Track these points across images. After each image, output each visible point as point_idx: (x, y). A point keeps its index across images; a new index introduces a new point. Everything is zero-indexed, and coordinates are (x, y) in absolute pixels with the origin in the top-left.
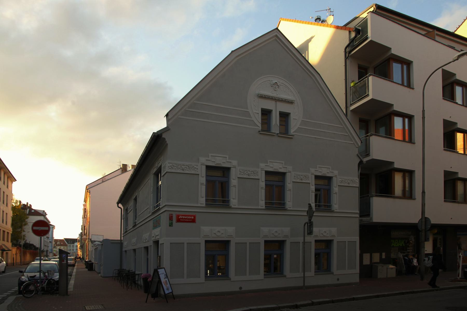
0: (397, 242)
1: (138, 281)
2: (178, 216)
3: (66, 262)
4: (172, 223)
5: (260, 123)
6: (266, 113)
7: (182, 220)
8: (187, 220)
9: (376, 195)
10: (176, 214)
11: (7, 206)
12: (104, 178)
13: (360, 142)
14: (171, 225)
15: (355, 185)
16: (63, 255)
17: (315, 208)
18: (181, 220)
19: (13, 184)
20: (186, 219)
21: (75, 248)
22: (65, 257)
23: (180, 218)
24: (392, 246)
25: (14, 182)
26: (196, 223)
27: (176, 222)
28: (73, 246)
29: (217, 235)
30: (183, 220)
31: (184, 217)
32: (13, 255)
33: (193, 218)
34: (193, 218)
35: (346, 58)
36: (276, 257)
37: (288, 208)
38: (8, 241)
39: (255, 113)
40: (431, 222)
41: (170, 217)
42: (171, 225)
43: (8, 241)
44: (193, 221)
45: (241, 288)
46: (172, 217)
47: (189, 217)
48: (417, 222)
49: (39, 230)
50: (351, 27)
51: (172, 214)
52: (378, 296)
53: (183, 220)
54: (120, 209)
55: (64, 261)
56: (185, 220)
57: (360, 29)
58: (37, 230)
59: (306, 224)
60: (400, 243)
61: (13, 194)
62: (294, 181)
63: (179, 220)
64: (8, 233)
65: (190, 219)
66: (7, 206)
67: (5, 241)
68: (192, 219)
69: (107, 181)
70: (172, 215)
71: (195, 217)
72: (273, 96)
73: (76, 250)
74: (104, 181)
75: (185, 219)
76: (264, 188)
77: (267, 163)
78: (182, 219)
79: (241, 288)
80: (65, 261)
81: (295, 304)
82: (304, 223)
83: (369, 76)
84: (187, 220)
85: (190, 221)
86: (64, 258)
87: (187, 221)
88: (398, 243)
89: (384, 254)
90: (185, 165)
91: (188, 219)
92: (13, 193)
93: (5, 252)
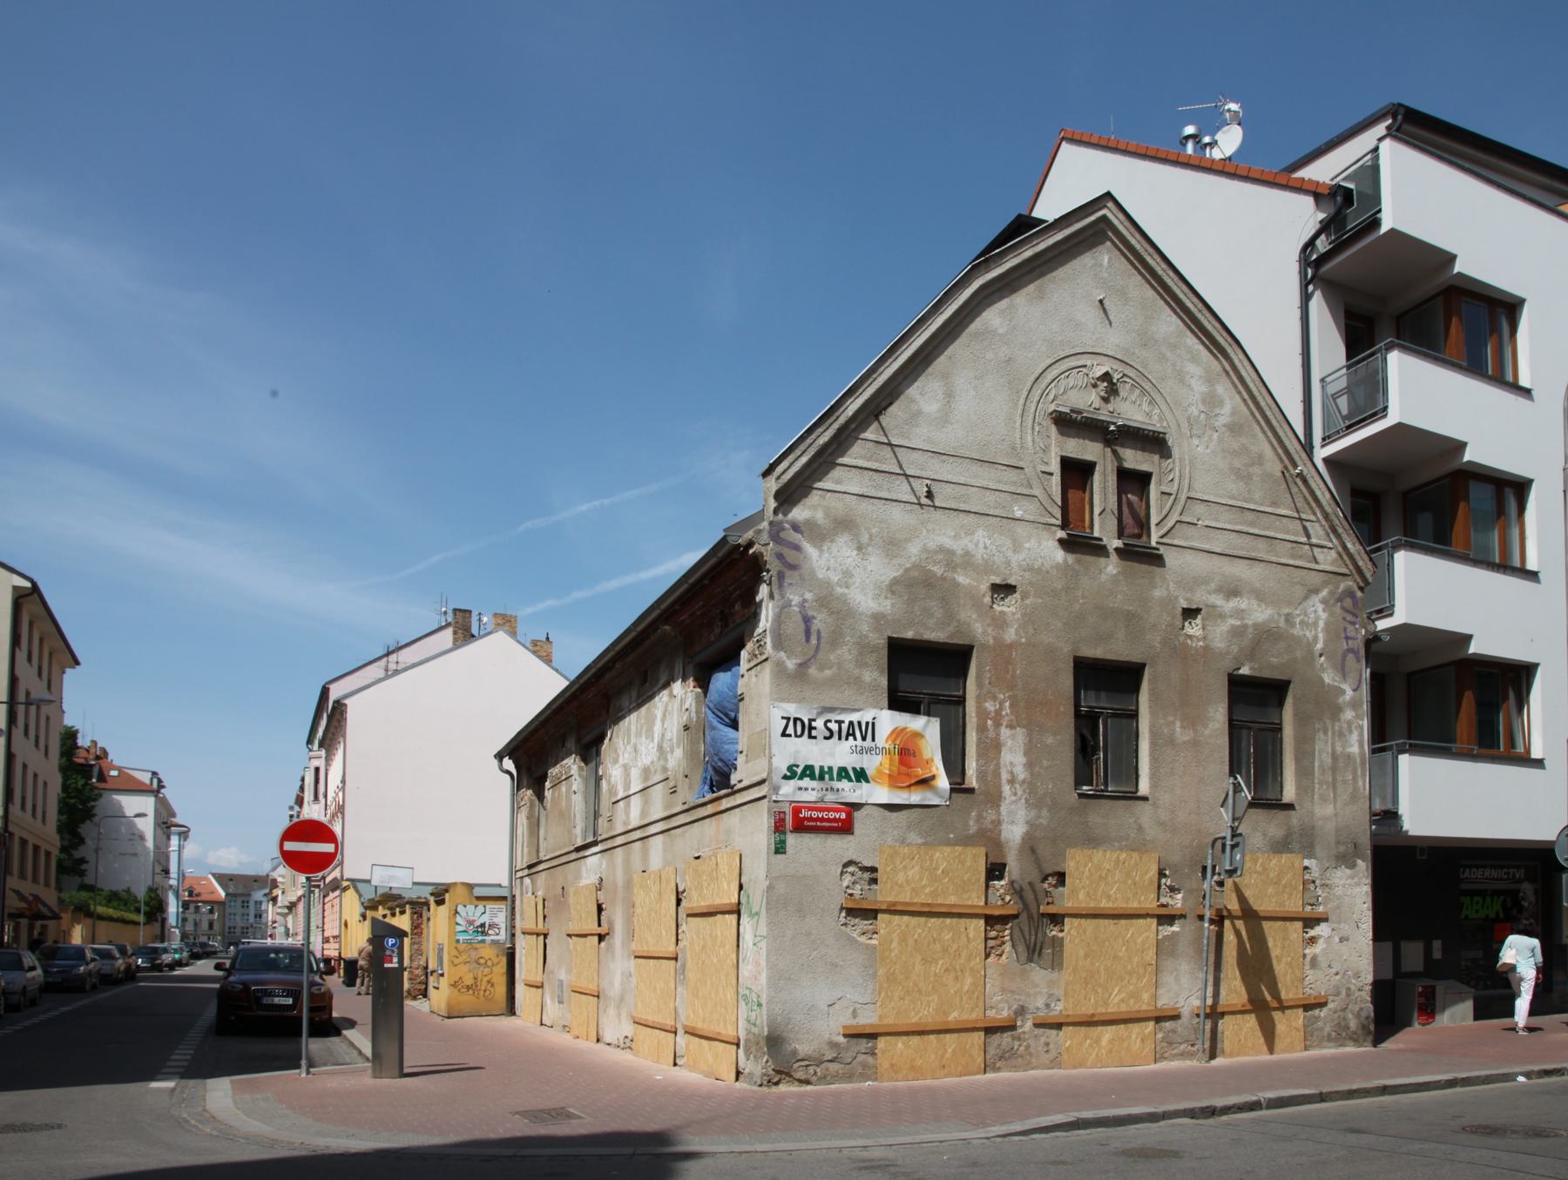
0: (1478, 903)
1: (1214, 1014)
3: (396, 965)
5: (1056, 504)
6: (1076, 473)
9: (1410, 745)
11: (46, 754)
12: (393, 658)
16: (388, 941)
19: (65, 675)
20: (822, 820)
21: (252, 912)
22: (393, 945)
23: (805, 819)
24: (1463, 917)
25: (68, 671)
28: (243, 902)
30: (812, 824)
31: (815, 814)
32: (62, 934)
35: (1305, 283)
36: (1434, 957)
38: (47, 884)
40: (70, 667)
43: (47, 884)
48: (1554, 839)
50: (1321, 182)
53: (812, 824)
54: (507, 777)
55: (391, 962)
56: (818, 823)
57: (1351, 190)
60: (1488, 908)
61: (64, 712)
64: (48, 854)
65: (835, 820)
66: (46, 754)
67: (39, 883)
68: (839, 820)
69: (406, 669)
73: (256, 916)
74: (397, 672)
75: (818, 819)
78: (811, 819)
80: (395, 960)
83: (1389, 348)
85: (836, 827)
86: (393, 951)
87: (824, 826)
88: (1483, 907)
89: (1437, 945)
91: (829, 820)
92: (64, 708)
93: (39, 923)
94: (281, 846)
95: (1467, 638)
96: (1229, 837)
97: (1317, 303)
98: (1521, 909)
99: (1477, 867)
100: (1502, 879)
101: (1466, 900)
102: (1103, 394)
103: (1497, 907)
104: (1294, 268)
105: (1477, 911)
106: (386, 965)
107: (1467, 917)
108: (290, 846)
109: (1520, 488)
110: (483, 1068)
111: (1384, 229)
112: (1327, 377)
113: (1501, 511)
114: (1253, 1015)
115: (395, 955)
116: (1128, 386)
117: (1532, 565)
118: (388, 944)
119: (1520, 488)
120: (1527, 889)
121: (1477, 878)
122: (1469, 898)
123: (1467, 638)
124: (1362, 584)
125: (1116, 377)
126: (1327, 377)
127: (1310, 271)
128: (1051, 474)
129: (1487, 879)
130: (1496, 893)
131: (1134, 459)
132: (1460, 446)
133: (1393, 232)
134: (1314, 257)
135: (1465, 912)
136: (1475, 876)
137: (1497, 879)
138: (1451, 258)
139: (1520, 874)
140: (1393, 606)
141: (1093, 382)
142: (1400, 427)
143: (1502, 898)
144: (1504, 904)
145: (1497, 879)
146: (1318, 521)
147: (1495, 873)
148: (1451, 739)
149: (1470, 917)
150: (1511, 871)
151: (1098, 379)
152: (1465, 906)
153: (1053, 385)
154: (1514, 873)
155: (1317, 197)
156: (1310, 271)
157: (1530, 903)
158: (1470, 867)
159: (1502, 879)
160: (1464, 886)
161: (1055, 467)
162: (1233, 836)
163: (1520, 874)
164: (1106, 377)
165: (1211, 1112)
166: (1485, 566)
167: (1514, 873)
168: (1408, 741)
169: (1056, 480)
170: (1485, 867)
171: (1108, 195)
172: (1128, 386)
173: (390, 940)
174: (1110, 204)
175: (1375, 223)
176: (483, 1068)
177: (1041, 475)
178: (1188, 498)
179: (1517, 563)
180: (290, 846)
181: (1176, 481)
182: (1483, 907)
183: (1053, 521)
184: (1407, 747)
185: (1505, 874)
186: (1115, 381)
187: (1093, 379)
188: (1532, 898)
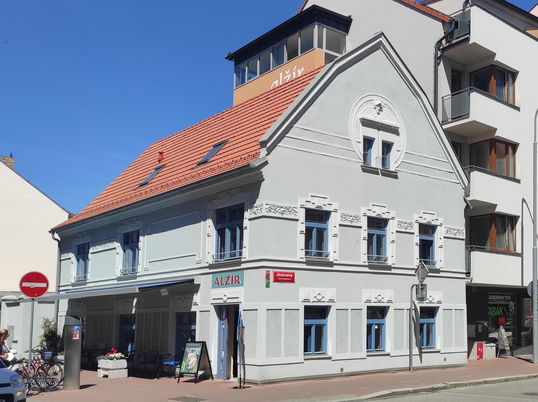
0: (494, 309)
2: (275, 274)
4: (269, 283)
6: (368, 143)
7: (280, 279)
8: (285, 279)
10: (273, 271)
13: (468, 182)
14: (268, 286)
15: (461, 237)
17: (368, 262)
18: (279, 279)
20: (284, 277)
22: (77, 329)
23: (278, 277)
26: (294, 283)
27: (273, 282)
29: (379, 300)
31: (282, 275)
33: (292, 276)
34: (292, 276)
35: (437, 59)
36: (377, 328)
37: (334, 261)
39: (357, 142)
41: (266, 275)
42: (268, 286)
44: (292, 280)
45: (342, 369)
46: (269, 274)
47: (288, 275)
49: (31, 287)
51: (269, 271)
52: (507, 380)
56: (283, 279)
58: (29, 288)
59: (415, 287)
62: (399, 230)
63: (276, 280)
70: (269, 272)
71: (293, 274)
72: (384, 123)
75: (283, 277)
76: (305, 232)
77: (369, 207)
78: (280, 277)
79: (342, 369)
81: (431, 387)
82: (412, 285)
84: (285, 279)
88: (496, 311)
90: (284, 207)
91: (287, 277)
94: (21, 284)
95: (495, 206)
96: (420, 285)
97: (441, 68)
98: (509, 312)
99: (494, 295)
100: (502, 300)
101: (490, 308)
102: (378, 111)
103: (501, 311)
104: (433, 50)
105: (494, 313)
106: (73, 338)
107: (490, 315)
108: (25, 284)
109: (515, 146)
110: (421, 363)
111: (471, 42)
112: (444, 97)
113: (507, 152)
114: (245, 364)
115: (78, 333)
116: (386, 108)
117: (517, 177)
118: (75, 329)
119: (515, 146)
120: (512, 304)
121: (493, 299)
122: (491, 307)
123: (495, 206)
124: (464, 187)
125: (382, 105)
126: (444, 97)
127: (439, 53)
128: (360, 143)
129: (497, 300)
130: (501, 305)
131: (389, 137)
132: (495, 130)
133: (474, 44)
134: (441, 47)
135: (489, 313)
136: (494, 298)
137: (501, 300)
138: (494, 55)
139: (509, 298)
140: (470, 192)
141: (375, 107)
142: (474, 122)
143: (503, 308)
144: (503, 310)
145: (501, 300)
146: (450, 162)
147: (500, 298)
148: (484, 244)
149: (491, 315)
150: (506, 296)
151: (376, 106)
152: (489, 311)
153: (361, 107)
154: (507, 297)
155: (443, 22)
156: (439, 53)
157: (513, 310)
158: (491, 295)
159: (502, 300)
160: (490, 303)
161: (361, 140)
162: (422, 285)
163: (509, 298)
164: (379, 105)
165: (434, 390)
166: (500, 177)
167: (507, 297)
168: (469, 246)
169: (362, 145)
170: (496, 295)
171: (383, 34)
172: (386, 108)
173: (76, 327)
174: (382, 36)
175: (468, 39)
176: (421, 363)
177: (356, 142)
178: (406, 152)
179: (511, 176)
180: (25, 284)
181: (402, 146)
182: (496, 311)
183: (360, 161)
184: (474, 248)
185: (504, 298)
186: (382, 106)
187: (375, 105)
188: (513, 308)
